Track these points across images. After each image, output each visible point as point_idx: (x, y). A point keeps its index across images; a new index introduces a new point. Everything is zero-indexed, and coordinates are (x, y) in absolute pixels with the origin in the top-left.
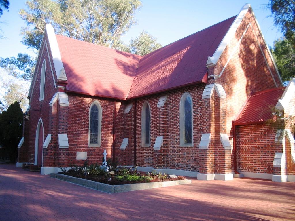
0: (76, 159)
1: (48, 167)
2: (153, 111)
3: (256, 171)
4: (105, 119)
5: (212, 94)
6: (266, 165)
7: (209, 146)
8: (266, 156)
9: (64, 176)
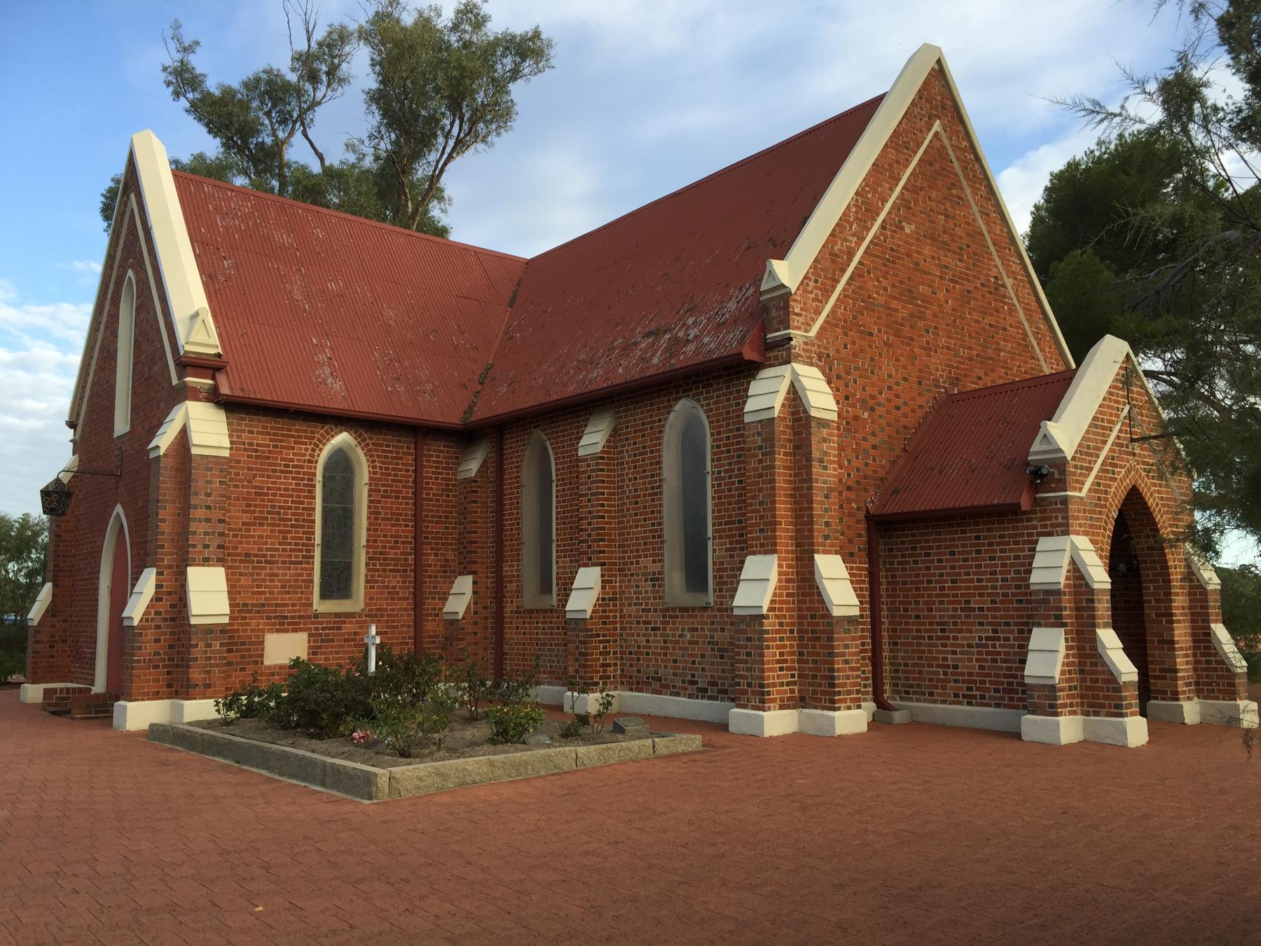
0: (262, 663)
1: (143, 700)
2: (563, 469)
3: (961, 699)
4: (379, 502)
5: (783, 405)
6: (997, 676)
7: (772, 602)
8: (998, 639)
9: (203, 734)
